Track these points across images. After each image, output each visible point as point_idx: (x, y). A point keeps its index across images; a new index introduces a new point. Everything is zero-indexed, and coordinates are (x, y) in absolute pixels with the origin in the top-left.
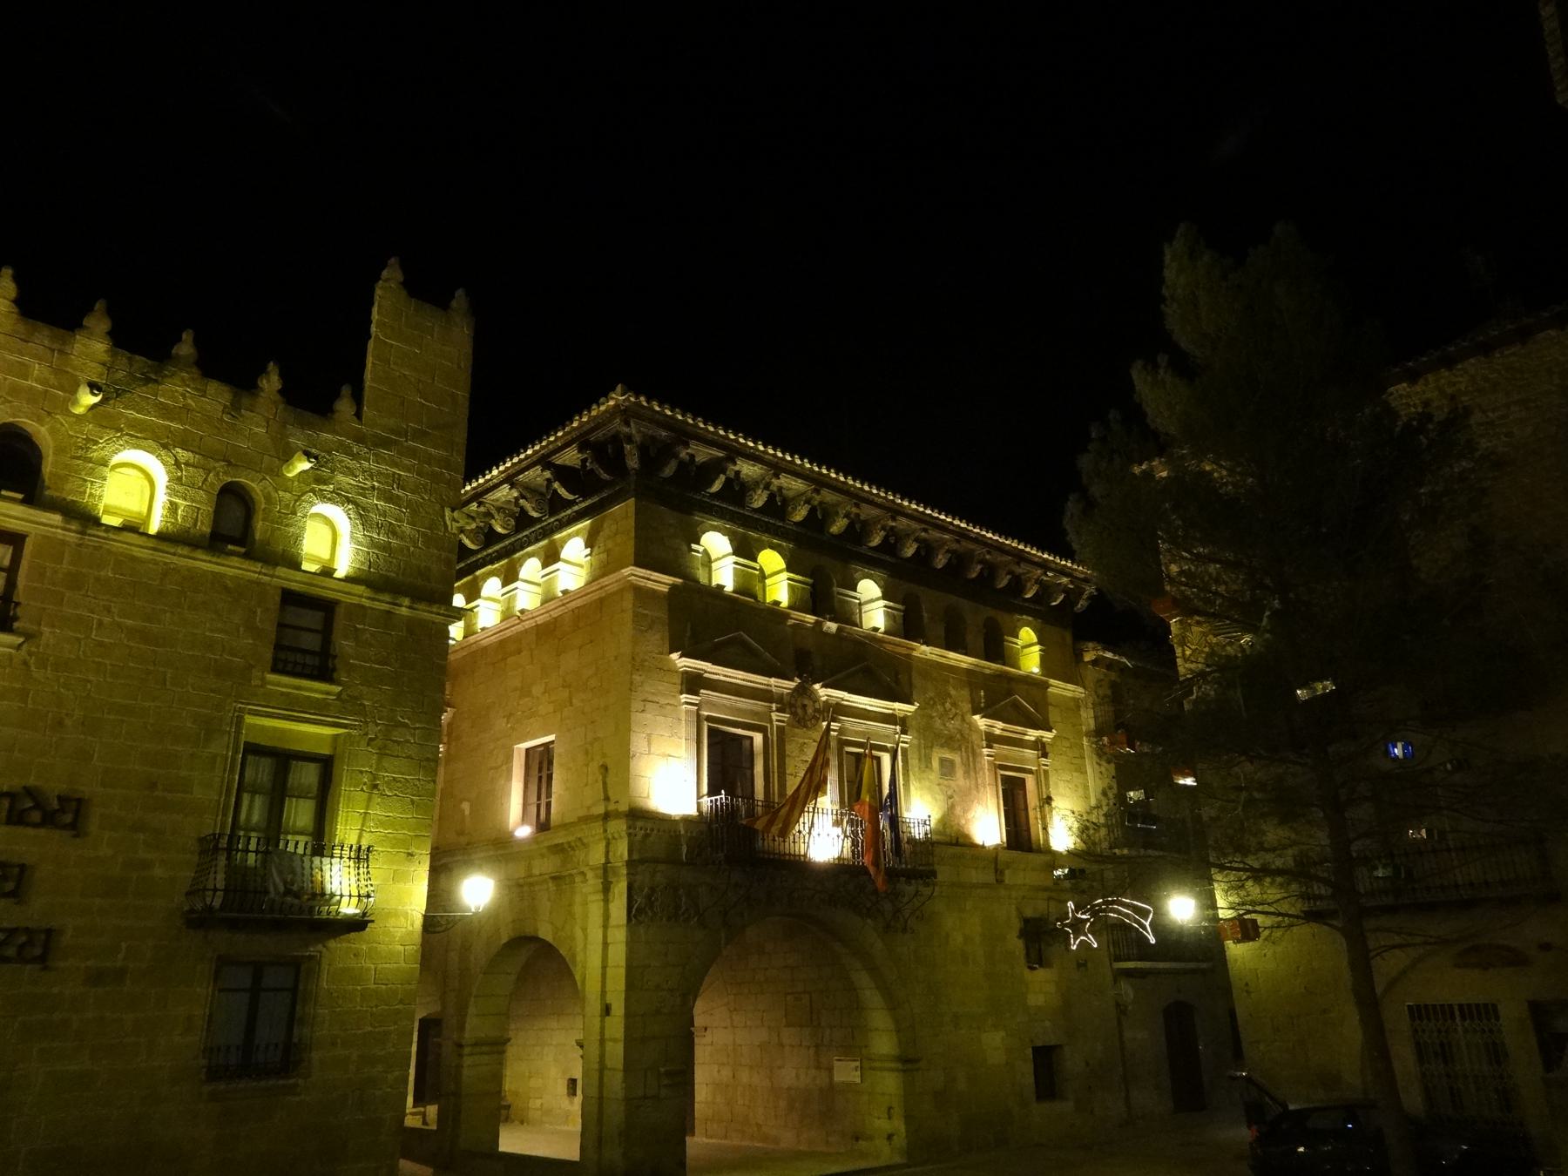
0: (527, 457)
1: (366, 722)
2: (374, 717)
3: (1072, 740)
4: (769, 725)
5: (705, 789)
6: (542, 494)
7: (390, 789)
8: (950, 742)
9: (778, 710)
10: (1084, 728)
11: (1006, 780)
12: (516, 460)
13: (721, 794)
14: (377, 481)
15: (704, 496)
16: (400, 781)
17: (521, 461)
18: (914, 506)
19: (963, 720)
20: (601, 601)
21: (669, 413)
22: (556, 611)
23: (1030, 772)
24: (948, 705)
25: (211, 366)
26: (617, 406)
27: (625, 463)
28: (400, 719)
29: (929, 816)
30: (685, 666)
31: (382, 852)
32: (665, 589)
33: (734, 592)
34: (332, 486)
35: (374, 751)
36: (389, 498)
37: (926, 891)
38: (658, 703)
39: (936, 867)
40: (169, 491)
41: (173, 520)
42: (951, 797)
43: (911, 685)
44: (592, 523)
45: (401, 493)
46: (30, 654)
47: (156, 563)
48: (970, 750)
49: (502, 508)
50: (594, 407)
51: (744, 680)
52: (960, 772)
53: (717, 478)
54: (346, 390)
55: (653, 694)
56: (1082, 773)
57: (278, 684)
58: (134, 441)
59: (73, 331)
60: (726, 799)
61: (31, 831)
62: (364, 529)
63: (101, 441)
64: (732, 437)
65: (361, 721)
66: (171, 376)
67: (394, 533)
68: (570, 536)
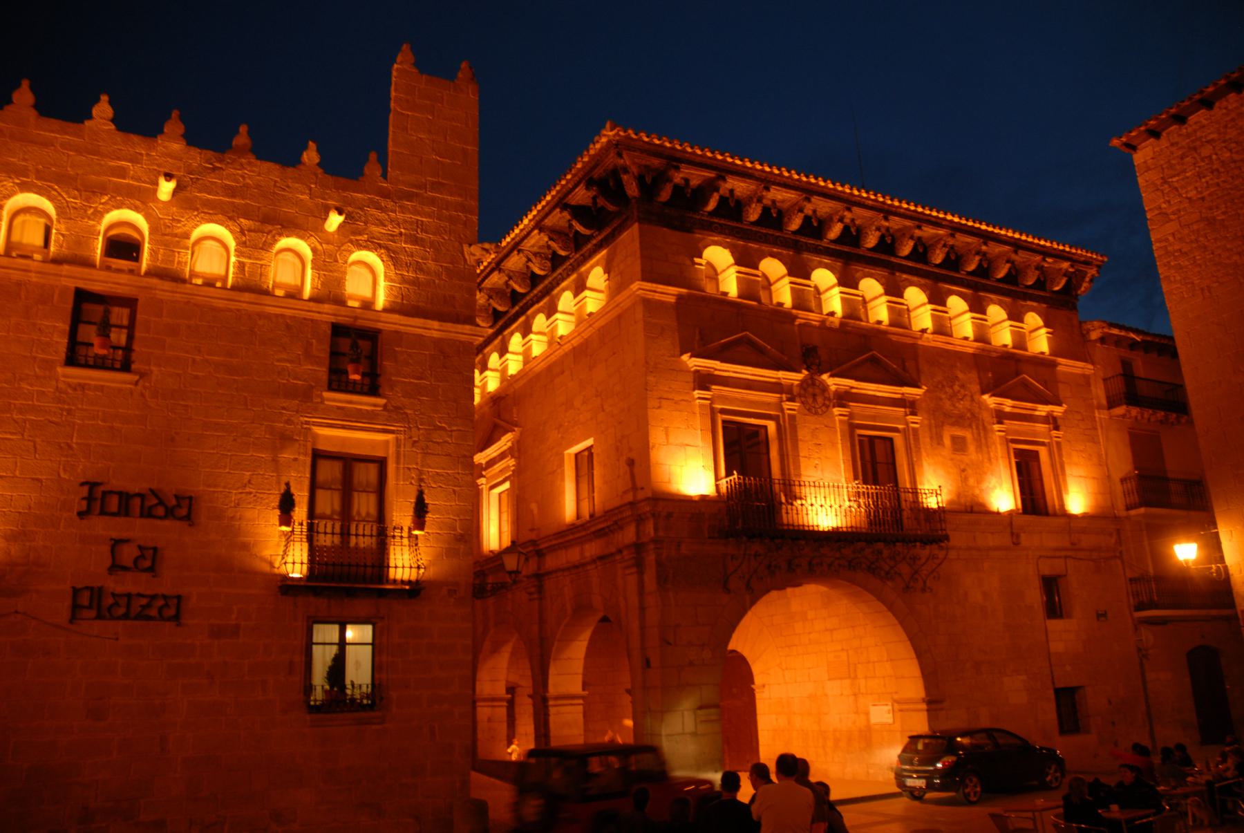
0: (548, 203)
1: (410, 428)
2: (416, 423)
3: (1084, 413)
4: (780, 414)
5: (723, 472)
6: (567, 235)
7: (435, 482)
8: (959, 420)
9: (789, 400)
10: (1095, 402)
11: (1018, 453)
12: (539, 207)
13: (733, 474)
14: (404, 228)
15: (703, 215)
16: (443, 475)
17: (544, 207)
18: (905, 206)
19: (973, 400)
20: (619, 317)
21: (657, 142)
22: (586, 332)
23: (1043, 444)
24: (956, 388)
25: (263, 150)
26: (609, 142)
27: (625, 192)
28: (439, 424)
29: (940, 487)
30: (696, 366)
31: (433, 533)
32: (672, 300)
33: (739, 297)
34: (366, 236)
35: (418, 451)
36: (415, 241)
37: (941, 554)
38: (673, 399)
39: (949, 533)
40: (237, 253)
41: (242, 276)
42: (963, 470)
43: (918, 371)
44: (608, 253)
45: (424, 236)
46: (145, 387)
47: (230, 310)
48: (981, 427)
49: (538, 253)
50: (591, 146)
51: (753, 375)
52: (972, 448)
53: (711, 196)
54: (373, 156)
55: (667, 392)
56: (1094, 442)
57: (334, 400)
58: (207, 217)
59: (156, 137)
60: (739, 478)
61: (159, 522)
62: (395, 269)
63: (183, 220)
64: (720, 157)
65: (405, 427)
66: (231, 164)
67: (421, 270)
68: (592, 267)
